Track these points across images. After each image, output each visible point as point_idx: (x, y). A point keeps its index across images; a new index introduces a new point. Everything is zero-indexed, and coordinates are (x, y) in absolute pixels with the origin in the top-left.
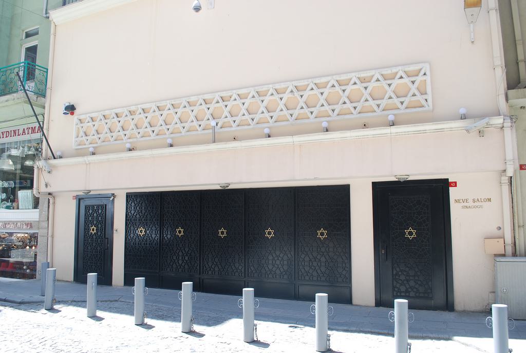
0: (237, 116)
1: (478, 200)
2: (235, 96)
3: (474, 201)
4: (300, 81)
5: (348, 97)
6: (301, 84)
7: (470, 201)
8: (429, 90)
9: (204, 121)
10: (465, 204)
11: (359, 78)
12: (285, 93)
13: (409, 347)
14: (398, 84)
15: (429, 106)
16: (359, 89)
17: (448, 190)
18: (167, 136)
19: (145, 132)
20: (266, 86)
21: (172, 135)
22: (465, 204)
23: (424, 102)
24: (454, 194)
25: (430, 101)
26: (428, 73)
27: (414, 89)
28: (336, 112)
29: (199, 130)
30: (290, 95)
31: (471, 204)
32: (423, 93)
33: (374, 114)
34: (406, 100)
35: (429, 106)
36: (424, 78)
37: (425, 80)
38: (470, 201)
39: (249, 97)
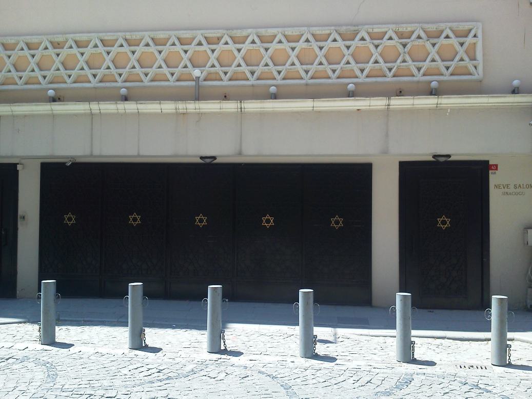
0: (73, 69)
1: (520, 186)
2: (22, 45)
3: (515, 187)
4: (324, 28)
5: (138, 61)
6: (109, 38)
7: (512, 187)
8: (479, 55)
9: (26, 73)
10: (506, 190)
11: (51, 42)
12: (87, 47)
13: (412, 345)
14: (68, 55)
15: (478, 74)
16: (206, 51)
17: (489, 172)
18: (119, 84)
19: (79, 76)
20: (16, 38)
21: (128, 84)
22: (506, 190)
23: (472, 69)
24: (494, 179)
25: (480, 68)
26: (480, 35)
27: (108, 60)
28: (365, 73)
29: (19, 83)
30: (305, 45)
31: (512, 190)
32: (473, 58)
33: (330, 81)
34: (453, 64)
35: (478, 74)
36: (475, 40)
37: (475, 44)
38: (512, 187)
39: (141, 44)
